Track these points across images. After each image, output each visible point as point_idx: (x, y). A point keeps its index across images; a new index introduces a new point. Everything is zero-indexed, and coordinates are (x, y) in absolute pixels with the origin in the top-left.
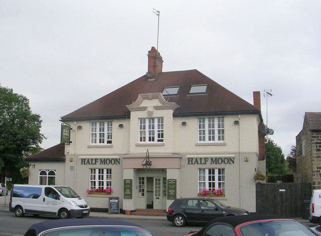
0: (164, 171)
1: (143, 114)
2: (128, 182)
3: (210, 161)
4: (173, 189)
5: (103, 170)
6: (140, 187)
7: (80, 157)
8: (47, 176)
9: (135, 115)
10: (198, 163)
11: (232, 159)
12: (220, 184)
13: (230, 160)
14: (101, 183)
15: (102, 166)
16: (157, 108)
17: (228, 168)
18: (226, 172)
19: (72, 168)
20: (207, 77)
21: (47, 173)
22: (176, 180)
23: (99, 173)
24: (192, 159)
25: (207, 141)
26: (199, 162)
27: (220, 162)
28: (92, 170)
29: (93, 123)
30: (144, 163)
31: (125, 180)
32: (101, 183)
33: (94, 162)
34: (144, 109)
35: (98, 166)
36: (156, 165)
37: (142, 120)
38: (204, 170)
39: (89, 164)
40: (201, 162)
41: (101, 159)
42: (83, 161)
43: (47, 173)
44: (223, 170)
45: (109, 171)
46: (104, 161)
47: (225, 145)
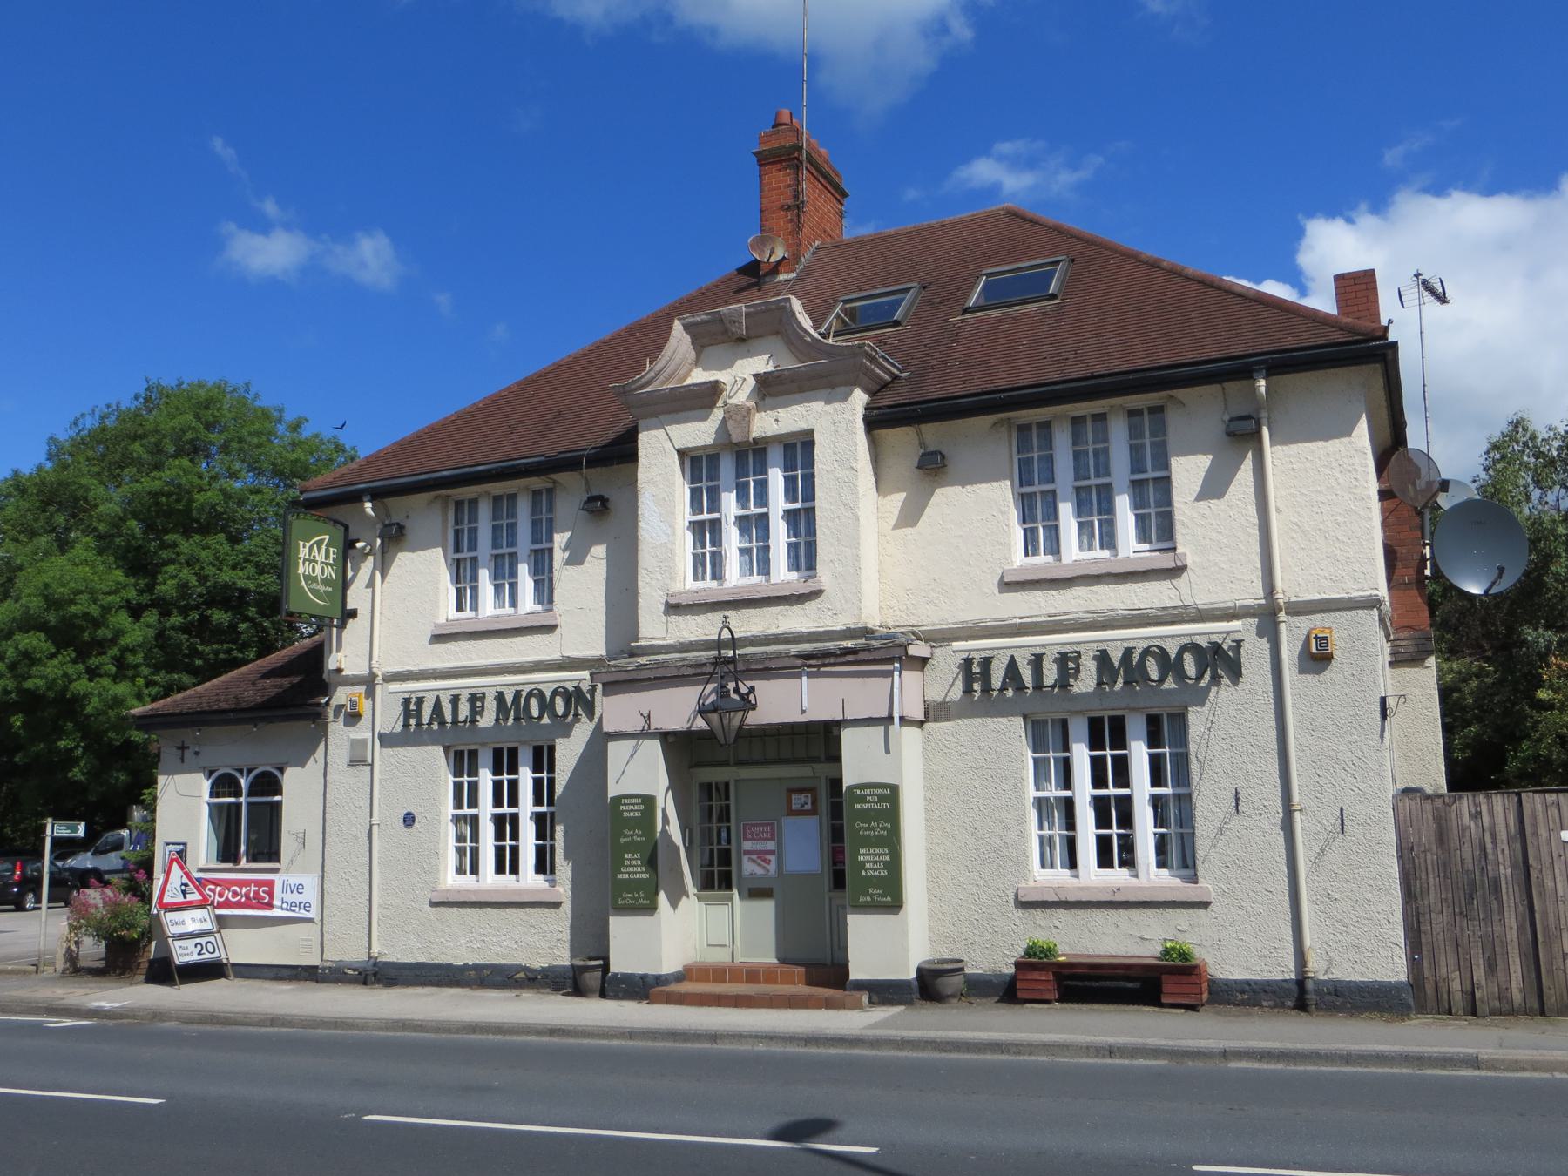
1: (700, 432)
4: (879, 842)
19: (358, 760)
32: (506, 794)
37: (697, 464)
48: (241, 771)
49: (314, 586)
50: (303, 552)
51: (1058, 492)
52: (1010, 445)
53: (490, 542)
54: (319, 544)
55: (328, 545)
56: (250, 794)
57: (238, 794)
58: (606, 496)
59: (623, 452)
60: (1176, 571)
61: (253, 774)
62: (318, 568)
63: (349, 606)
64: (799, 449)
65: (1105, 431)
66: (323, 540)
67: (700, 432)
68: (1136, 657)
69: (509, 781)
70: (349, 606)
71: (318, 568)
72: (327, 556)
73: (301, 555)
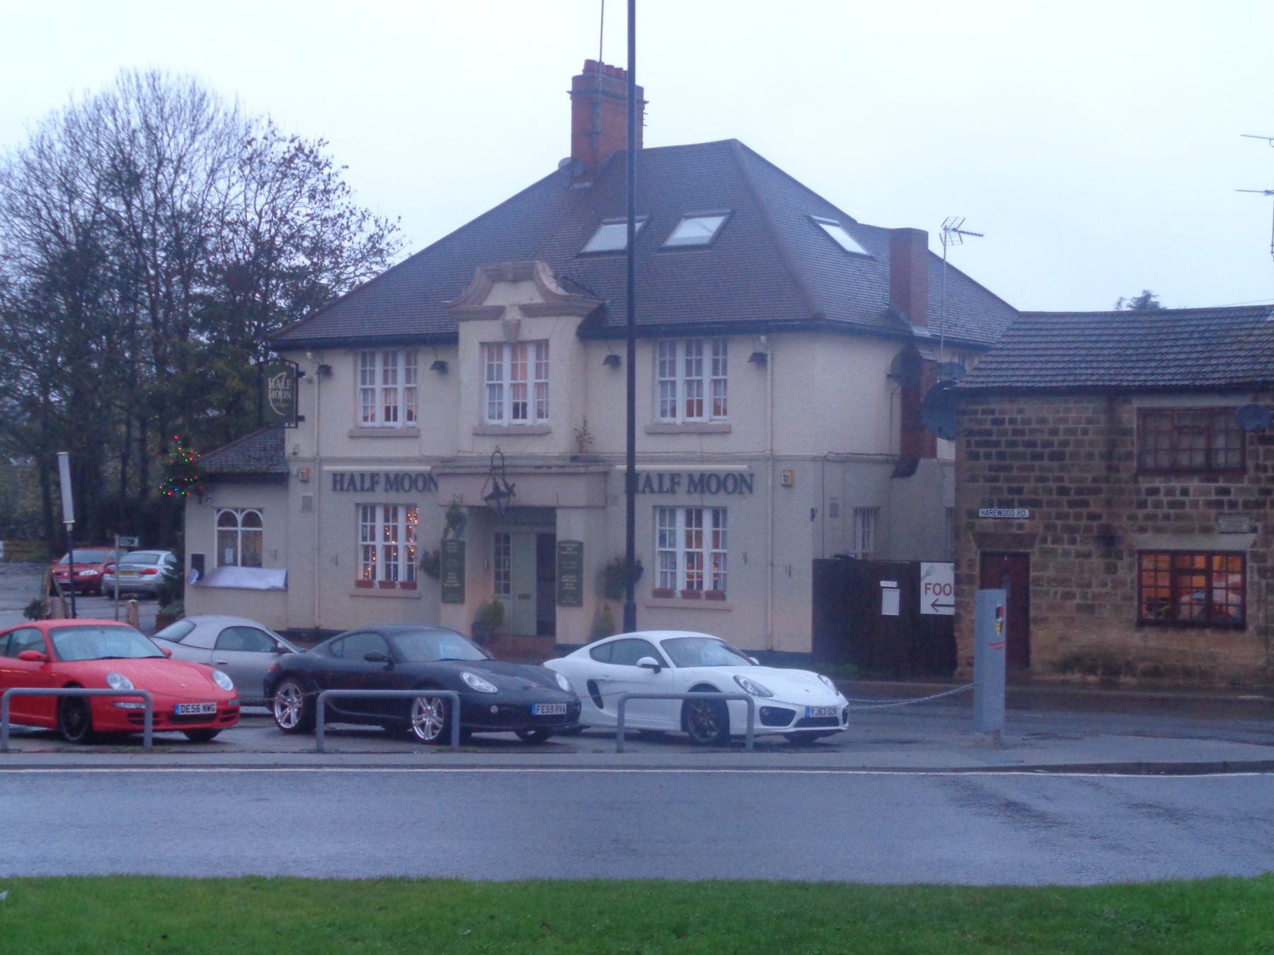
0: (547, 515)
1: (492, 331)
3: (685, 482)
6: (498, 564)
7: (326, 468)
8: (240, 529)
9: (472, 335)
10: (355, 489)
11: (748, 480)
12: (716, 557)
13: (742, 483)
14: (694, 538)
15: (392, 498)
16: (529, 311)
17: (735, 505)
18: (731, 519)
19: (307, 505)
22: (581, 544)
23: (387, 520)
24: (342, 475)
25: (681, 417)
26: (656, 486)
28: (365, 508)
29: (364, 355)
30: (489, 490)
32: (694, 538)
33: (667, 484)
34: (498, 312)
35: (380, 496)
36: (532, 493)
37: (492, 349)
38: (673, 511)
39: (652, 491)
40: (661, 485)
41: (690, 476)
42: (341, 482)
44: (725, 510)
45: (719, 515)
46: (701, 483)
48: (237, 511)
49: (278, 405)
50: (271, 385)
51: (729, 383)
52: (355, 375)
53: (711, 371)
54: (280, 378)
55: (287, 378)
56: (244, 524)
57: (235, 524)
58: (618, 355)
59: (450, 340)
60: (725, 432)
61: (245, 513)
62: (280, 393)
63: (300, 413)
64: (542, 346)
65: (502, 354)
66: (282, 376)
67: (492, 331)
68: (400, 478)
69: (696, 532)
70: (300, 413)
71: (280, 393)
72: (285, 385)
73: (270, 387)
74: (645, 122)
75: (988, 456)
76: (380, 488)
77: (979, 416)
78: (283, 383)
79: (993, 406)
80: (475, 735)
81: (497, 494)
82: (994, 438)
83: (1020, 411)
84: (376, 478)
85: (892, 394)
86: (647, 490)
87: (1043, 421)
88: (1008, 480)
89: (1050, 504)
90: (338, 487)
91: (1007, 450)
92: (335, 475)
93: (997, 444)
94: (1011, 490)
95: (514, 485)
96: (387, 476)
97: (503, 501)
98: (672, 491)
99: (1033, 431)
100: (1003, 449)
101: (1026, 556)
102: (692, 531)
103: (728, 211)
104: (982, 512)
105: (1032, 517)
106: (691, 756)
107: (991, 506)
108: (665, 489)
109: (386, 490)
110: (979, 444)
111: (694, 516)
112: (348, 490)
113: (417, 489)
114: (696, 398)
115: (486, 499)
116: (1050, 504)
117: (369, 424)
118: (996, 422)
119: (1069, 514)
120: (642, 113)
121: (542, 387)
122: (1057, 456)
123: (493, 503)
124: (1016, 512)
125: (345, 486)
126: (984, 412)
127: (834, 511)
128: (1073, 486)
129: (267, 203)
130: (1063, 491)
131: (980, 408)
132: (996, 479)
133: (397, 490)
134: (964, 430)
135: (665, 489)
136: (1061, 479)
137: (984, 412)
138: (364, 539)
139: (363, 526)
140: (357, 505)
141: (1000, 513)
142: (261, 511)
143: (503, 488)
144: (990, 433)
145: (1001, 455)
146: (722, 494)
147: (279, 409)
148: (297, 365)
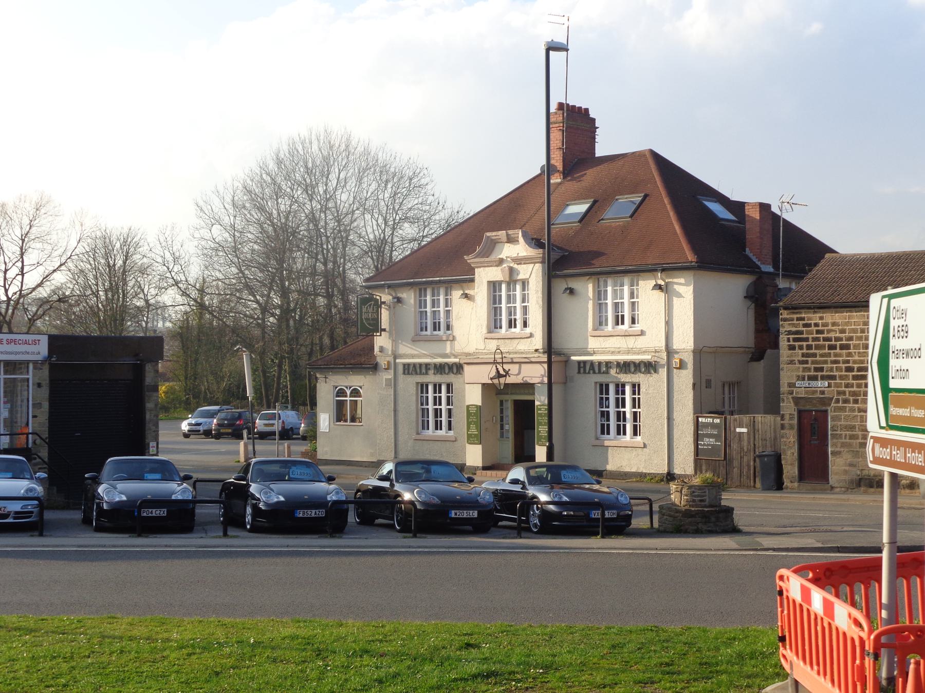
2: (473, 410)
5: (440, 386)
9: (485, 275)
15: (438, 379)
20: (684, 171)
21: (348, 392)
24: (409, 365)
26: (597, 370)
27: (447, 371)
30: (493, 373)
31: (468, 407)
33: (424, 371)
35: (432, 378)
37: (494, 286)
39: (594, 372)
43: (348, 392)
45: (636, 388)
46: (625, 367)
47: (642, 333)
48: (347, 388)
62: (370, 315)
64: (525, 284)
69: (622, 398)
71: (370, 315)
72: (373, 310)
74: (596, 140)
75: (801, 348)
76: (431, 372)
77: (795, 322)
78: (371, 308)
79: (803, 315)
80: (500, 523)
81: (499, 376)
82: (804, 336)
83: (821, 318)
84: (428, 367)
85: (748, 308)
86: (413, 373)
87: (834, 324)
88: (813, 363)
89: (841, 377)
90: (582, 370)
91: (813, 343)
92: (404, 365)
93: (807, 340)
94: (816, 370)
95: (509, 370)
96: (435, 365)
97: (502, 380)
98: (427, 373)
99: (829, 331)
100: (810, 343)
101: (826, 411)
102: (619, 398)
103: (643, 195)
104: (798, 384)
105: (829, 386)
106: (530, 543)
107: (803, 379)
108: (602, 371)
109: (434, 374)
110: (795, 340)
111: (437, 388)
112: (589, 373)
113: (453, 373)
114: (620, 314)
115: (491, 379)
116: (841, 377)
117: (424, 333)
118: (806, 325)
119: (853, 384)
120: (595, 135)
121: (525, 310)
122: (843, 347)
123: (496, 381)
124: (819, 383)
125: (410, 371)
126: (798, 319)
127: (708, 384)
128: (856, 366)
129: (390, 197)
130: (849, 369)
131: (795, 316)
132: (807, 362)
133: (441, 374)
134: (786, 331)
135: (602, 371)
136: (848, 362)
137: (798, 319)
138: (422, 404)
139: (421, 397)
140: (417, 383)
141: (809, 384)
142: (361, 388)
143: (502, 372)
144: (801, 333)
145: (809, 347)
146: (452, 375)
147: (369, 324)
148: (381, 297)
